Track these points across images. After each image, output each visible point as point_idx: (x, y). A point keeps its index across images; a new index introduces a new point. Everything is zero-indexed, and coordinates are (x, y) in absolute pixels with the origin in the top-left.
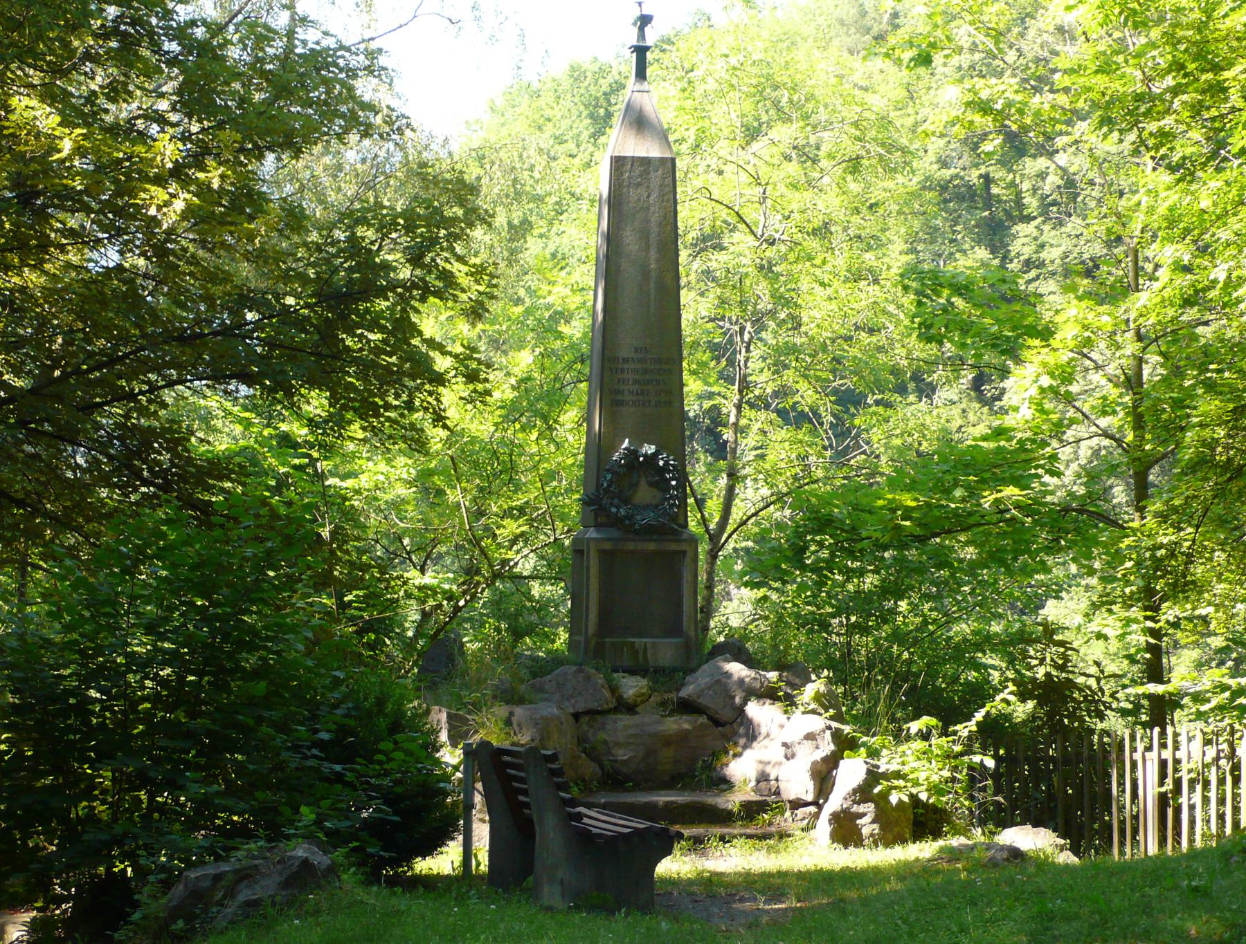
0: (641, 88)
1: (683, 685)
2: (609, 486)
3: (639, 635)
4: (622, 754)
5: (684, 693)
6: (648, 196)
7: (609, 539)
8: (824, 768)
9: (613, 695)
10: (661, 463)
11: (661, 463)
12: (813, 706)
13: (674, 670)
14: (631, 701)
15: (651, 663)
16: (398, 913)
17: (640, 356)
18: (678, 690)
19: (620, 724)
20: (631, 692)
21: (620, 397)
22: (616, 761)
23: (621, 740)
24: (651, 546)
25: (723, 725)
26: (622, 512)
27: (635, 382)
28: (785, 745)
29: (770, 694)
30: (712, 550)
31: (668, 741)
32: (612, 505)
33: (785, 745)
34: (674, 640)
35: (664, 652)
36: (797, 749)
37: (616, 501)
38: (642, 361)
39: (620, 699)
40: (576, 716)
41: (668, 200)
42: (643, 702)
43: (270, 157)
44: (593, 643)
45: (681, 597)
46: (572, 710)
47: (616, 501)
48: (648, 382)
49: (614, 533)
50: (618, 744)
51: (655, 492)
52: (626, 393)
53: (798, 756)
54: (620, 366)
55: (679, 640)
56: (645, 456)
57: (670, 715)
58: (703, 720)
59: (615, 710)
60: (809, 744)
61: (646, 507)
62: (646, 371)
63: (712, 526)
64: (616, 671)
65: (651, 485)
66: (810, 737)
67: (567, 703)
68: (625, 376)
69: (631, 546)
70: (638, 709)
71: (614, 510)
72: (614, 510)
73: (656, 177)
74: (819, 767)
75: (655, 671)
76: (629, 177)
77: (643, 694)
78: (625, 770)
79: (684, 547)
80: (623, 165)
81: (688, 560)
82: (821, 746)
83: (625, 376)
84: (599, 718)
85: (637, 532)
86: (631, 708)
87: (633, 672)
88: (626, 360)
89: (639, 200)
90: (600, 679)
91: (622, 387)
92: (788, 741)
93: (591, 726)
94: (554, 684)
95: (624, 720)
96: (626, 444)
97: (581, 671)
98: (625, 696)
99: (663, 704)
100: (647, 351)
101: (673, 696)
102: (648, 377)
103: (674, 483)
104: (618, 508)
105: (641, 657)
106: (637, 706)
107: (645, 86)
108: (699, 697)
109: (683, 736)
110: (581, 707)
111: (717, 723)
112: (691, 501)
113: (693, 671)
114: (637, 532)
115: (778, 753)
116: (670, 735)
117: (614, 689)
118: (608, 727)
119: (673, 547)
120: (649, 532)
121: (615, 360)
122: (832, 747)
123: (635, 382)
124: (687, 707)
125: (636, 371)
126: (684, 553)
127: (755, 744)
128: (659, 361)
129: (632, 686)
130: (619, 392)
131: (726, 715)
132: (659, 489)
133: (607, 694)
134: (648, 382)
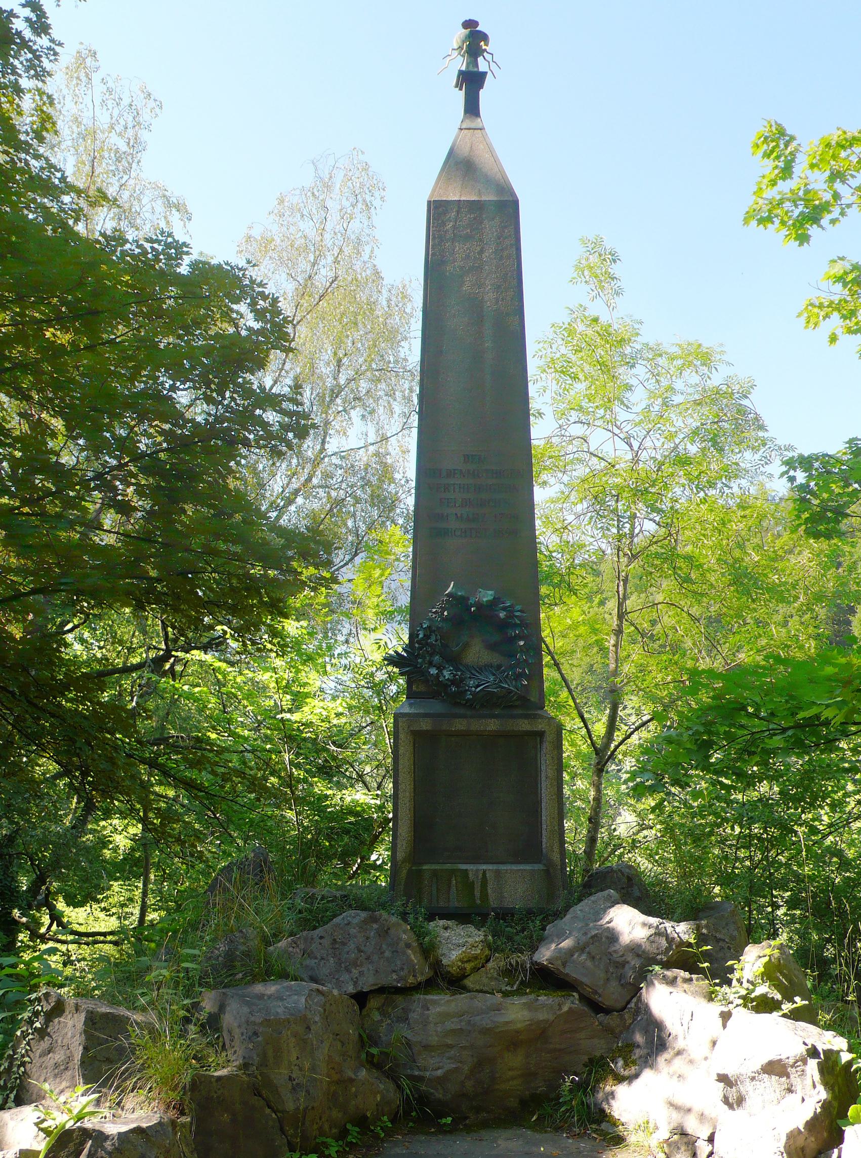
0: (473, 125)
1: (541, 940)
2: (427, 637)
3: (476, 860)
4: (435, 1066)
5: (545, 954)
6: (481, 252)
7: (426, 715)
8: (812, 1144)
9: (426, 958)
12: (762, 989)
13: (530, 913)
14: (454, 970)
15: (493, 902)
18: (534, 949)
19: (434, 1010)
20: (455, 955)
22: (420, 1079)
23: (434, 1040)
24: (492, 725)
25: (607, 1011)
26: (447, 674)
28: (723, 1078)
29: (683, 960)
30: (598, 764)
31: (513, 1041)
32: (431, 664)
33: (723, 1078)
34: (528, 867)
35: (513, 885)
36: (747, 1088)
37: (437, 659)
39: (437, 966)
40: (361, 998)
41: (509, 257)
42: (476, 969)
44: (404, 873)
45: (540, 802)
46: (351, 989)
47: (437, 659)
49: (436, 707)
50: (427, 1047)
53: (748, 1103)
55: (537, 867)
56: (479, 606)
57: (519, 992)
58: (571, 1003)
59: (429, 985)
60: (772, 1083)
61: (481, 669)
63: (599, 743)
64: (431, 917)
66: (775, 1068)
67: (345, 977)
69: (460, 725)
70: (468, 982)
71: (433, 671)
72: (433, 671)
73: (491, 228)
74: (801, 1142)
75: (484, 917)
76: (454, 227)
77: (476, 958)
78: (439, 1095)
79: (540, 726)
80: (445, 213)
81: (547, 746)
82: (798, 1087)
84: (399, 999)
85: (470, 705)
86: (454, 982)
87: (462, 917)
88: (451, 474)
89: (468, 257)
90: (405, 934)
92: (731, 1072)
93: (384, 1013)
94: (326, 942)
95: (442, 1004)
97: (374, 920)
98: (445, 961)
99: (509, 972)
101: (524, 958)
104: (440, 668)
105: (477, 893)
106: (465, 977)
107: (477, 123)
108: (564, 964)
109: (538, 1035)
110: (368, 982)
111: (597, 1008)
112: (547, 659)
113: (558, 915)
114: (470, 705)
115: (706, 1096)
116: (517, 1032)
117: (428, 951)
118: (413, 1016)
119: (524, 725)
120: (488, 703)
122: (822, 1094)
124: (547, 979)
126: (541, 734)
127: (661, 1060)
129: (458, 943)
131: (611, 994)
133: (414, 957)
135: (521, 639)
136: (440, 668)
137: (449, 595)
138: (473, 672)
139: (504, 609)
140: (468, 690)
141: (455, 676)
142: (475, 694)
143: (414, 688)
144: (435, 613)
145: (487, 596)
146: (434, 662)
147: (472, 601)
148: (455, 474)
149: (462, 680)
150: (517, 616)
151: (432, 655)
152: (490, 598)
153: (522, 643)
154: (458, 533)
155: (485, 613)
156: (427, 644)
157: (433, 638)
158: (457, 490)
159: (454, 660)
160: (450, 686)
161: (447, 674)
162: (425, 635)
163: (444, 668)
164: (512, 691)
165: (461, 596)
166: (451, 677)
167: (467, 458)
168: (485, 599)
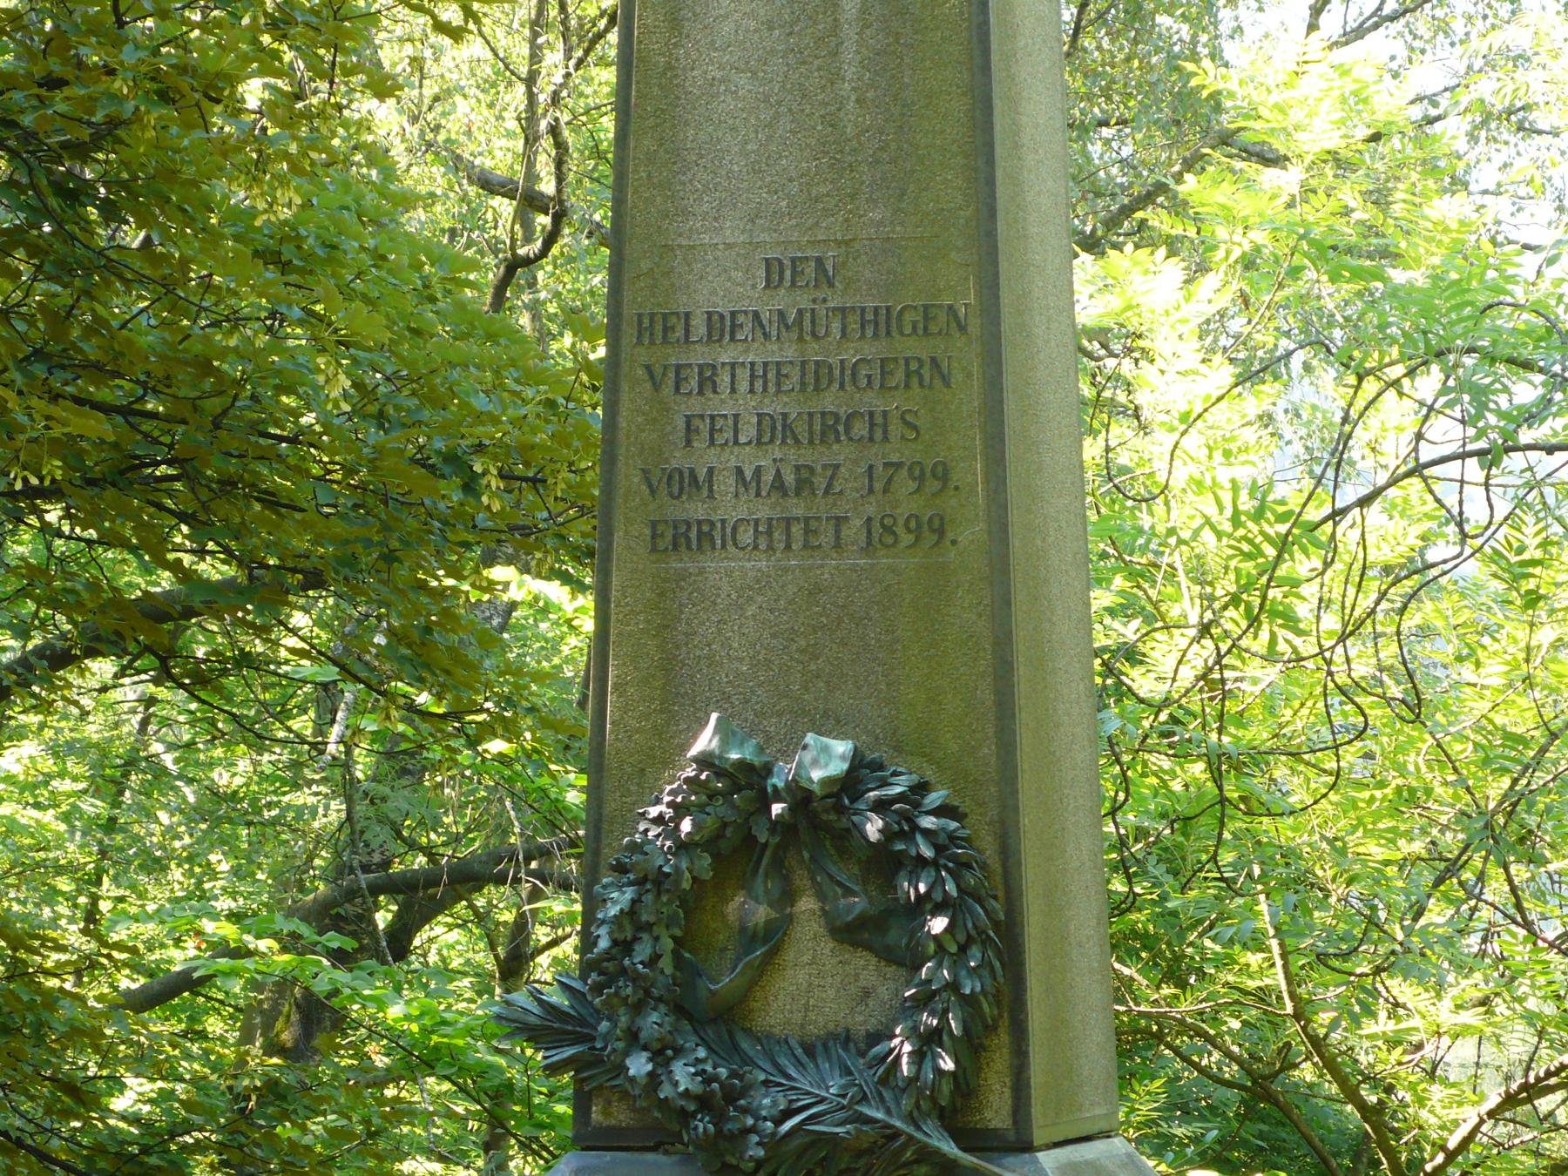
2: (623, 946)
10: (873, 828)
11: (873, 828)
16: (682, 576)
17: (786, 301)
21: (697, 510)
27: (774, 429)
32: (633, 1039)
37: (653, 1022)
38: (799, 326)
43: (583, 781)
47: (653, 1022)
48: (831, 429)
51: (866, 968)
52: (726, 484)
54: (699, 355)
56: (800, 796)
62: (818, 377)
65: (849, 933)
68: (722, 404)
83: (722, 404)
88: (722, 327)
91: (704, 458)
96: (706, 741)
100: (824, 278)
102: (830, 401)
103: (938, 925)
121: (664, 326)
123: (774, 429)
125: (766, 377)
128: (881, 322)
130: (689, 483)
132: (888, 955)
134: (831, 429)
135: (937, 910)
136: (663, 1054)
137: (704, 761)
138: (783, 1061)
139: (881, 806)
140: (753, 1130)
141: (708, 1080)
142: (774, 1144)
143: (596, 1115)
144: (659, 820)
145: (825, 759)
146: (643, 1035)
147: (777, 781)
148: (734, 327)
149: (732, 1096)
150: (927, 833)
151: (638, 1008)
152: (837, 768)
153: (938, 925)
154: (746, 536)
155: (821, 817)
156: (623, 971)
157: (643, 951)
158: (743, 386)
159: (723, 1023)
160: (693, 1115)
161: (683, 1076)
162: (615, 943)
163: (679, 1051)
164: (897, 1133)
165: (741, 764)
166: (696, 1087)
167: (774, 273)
168: (816, 775)
